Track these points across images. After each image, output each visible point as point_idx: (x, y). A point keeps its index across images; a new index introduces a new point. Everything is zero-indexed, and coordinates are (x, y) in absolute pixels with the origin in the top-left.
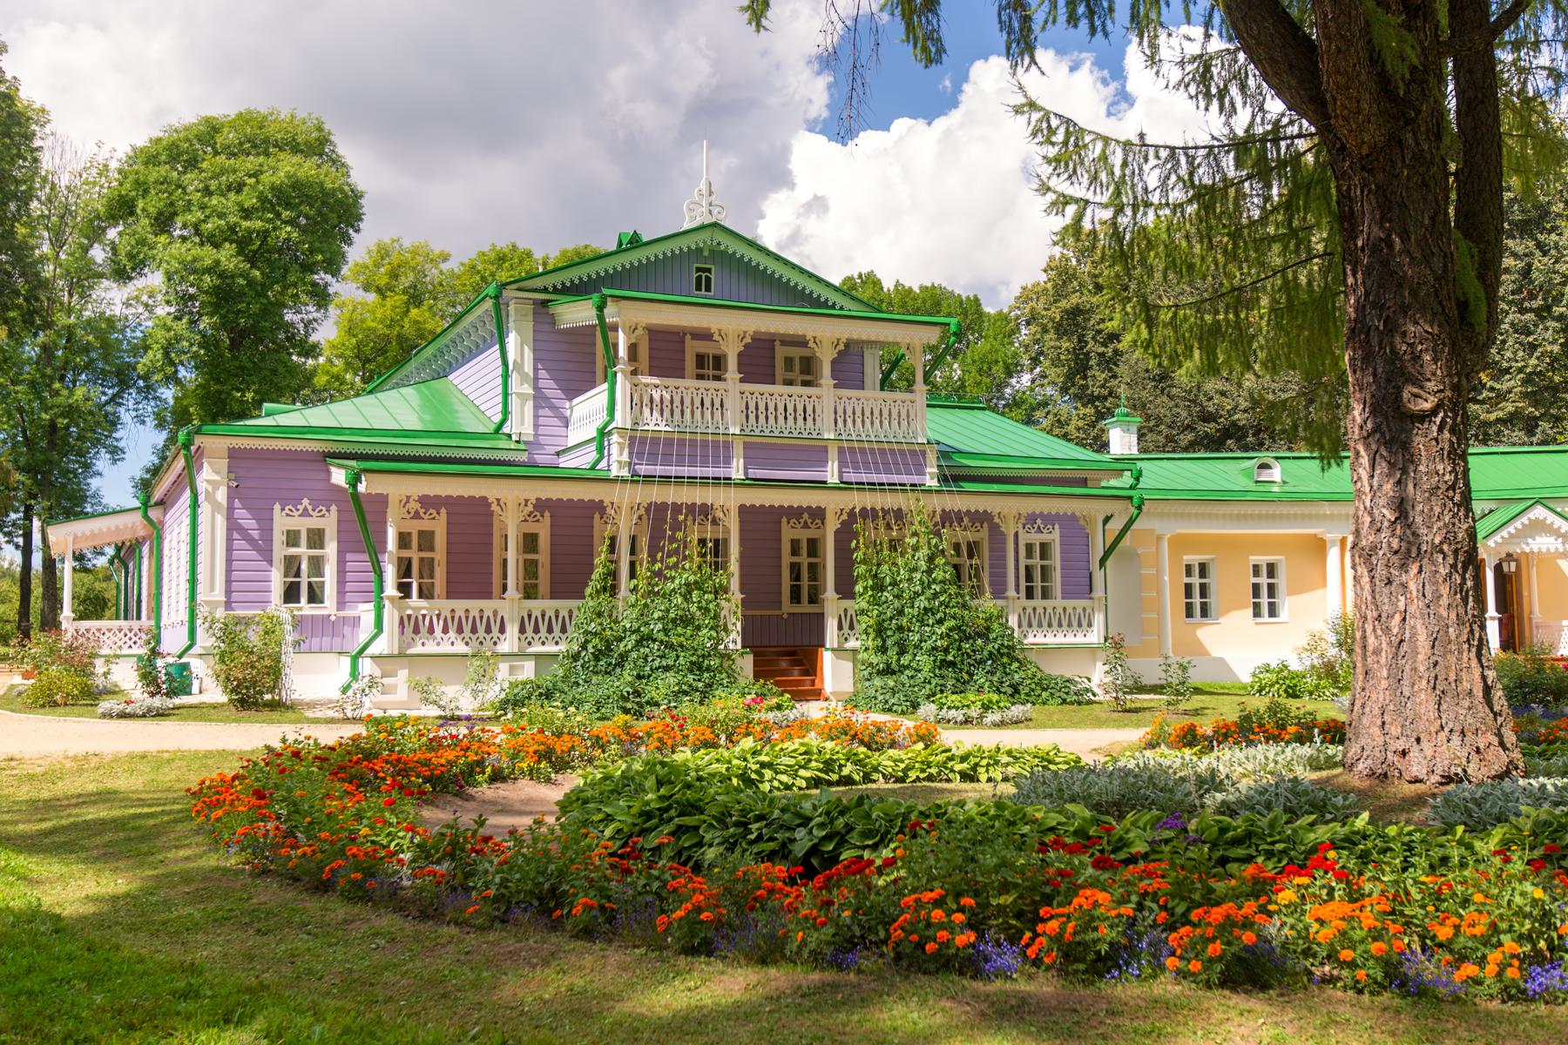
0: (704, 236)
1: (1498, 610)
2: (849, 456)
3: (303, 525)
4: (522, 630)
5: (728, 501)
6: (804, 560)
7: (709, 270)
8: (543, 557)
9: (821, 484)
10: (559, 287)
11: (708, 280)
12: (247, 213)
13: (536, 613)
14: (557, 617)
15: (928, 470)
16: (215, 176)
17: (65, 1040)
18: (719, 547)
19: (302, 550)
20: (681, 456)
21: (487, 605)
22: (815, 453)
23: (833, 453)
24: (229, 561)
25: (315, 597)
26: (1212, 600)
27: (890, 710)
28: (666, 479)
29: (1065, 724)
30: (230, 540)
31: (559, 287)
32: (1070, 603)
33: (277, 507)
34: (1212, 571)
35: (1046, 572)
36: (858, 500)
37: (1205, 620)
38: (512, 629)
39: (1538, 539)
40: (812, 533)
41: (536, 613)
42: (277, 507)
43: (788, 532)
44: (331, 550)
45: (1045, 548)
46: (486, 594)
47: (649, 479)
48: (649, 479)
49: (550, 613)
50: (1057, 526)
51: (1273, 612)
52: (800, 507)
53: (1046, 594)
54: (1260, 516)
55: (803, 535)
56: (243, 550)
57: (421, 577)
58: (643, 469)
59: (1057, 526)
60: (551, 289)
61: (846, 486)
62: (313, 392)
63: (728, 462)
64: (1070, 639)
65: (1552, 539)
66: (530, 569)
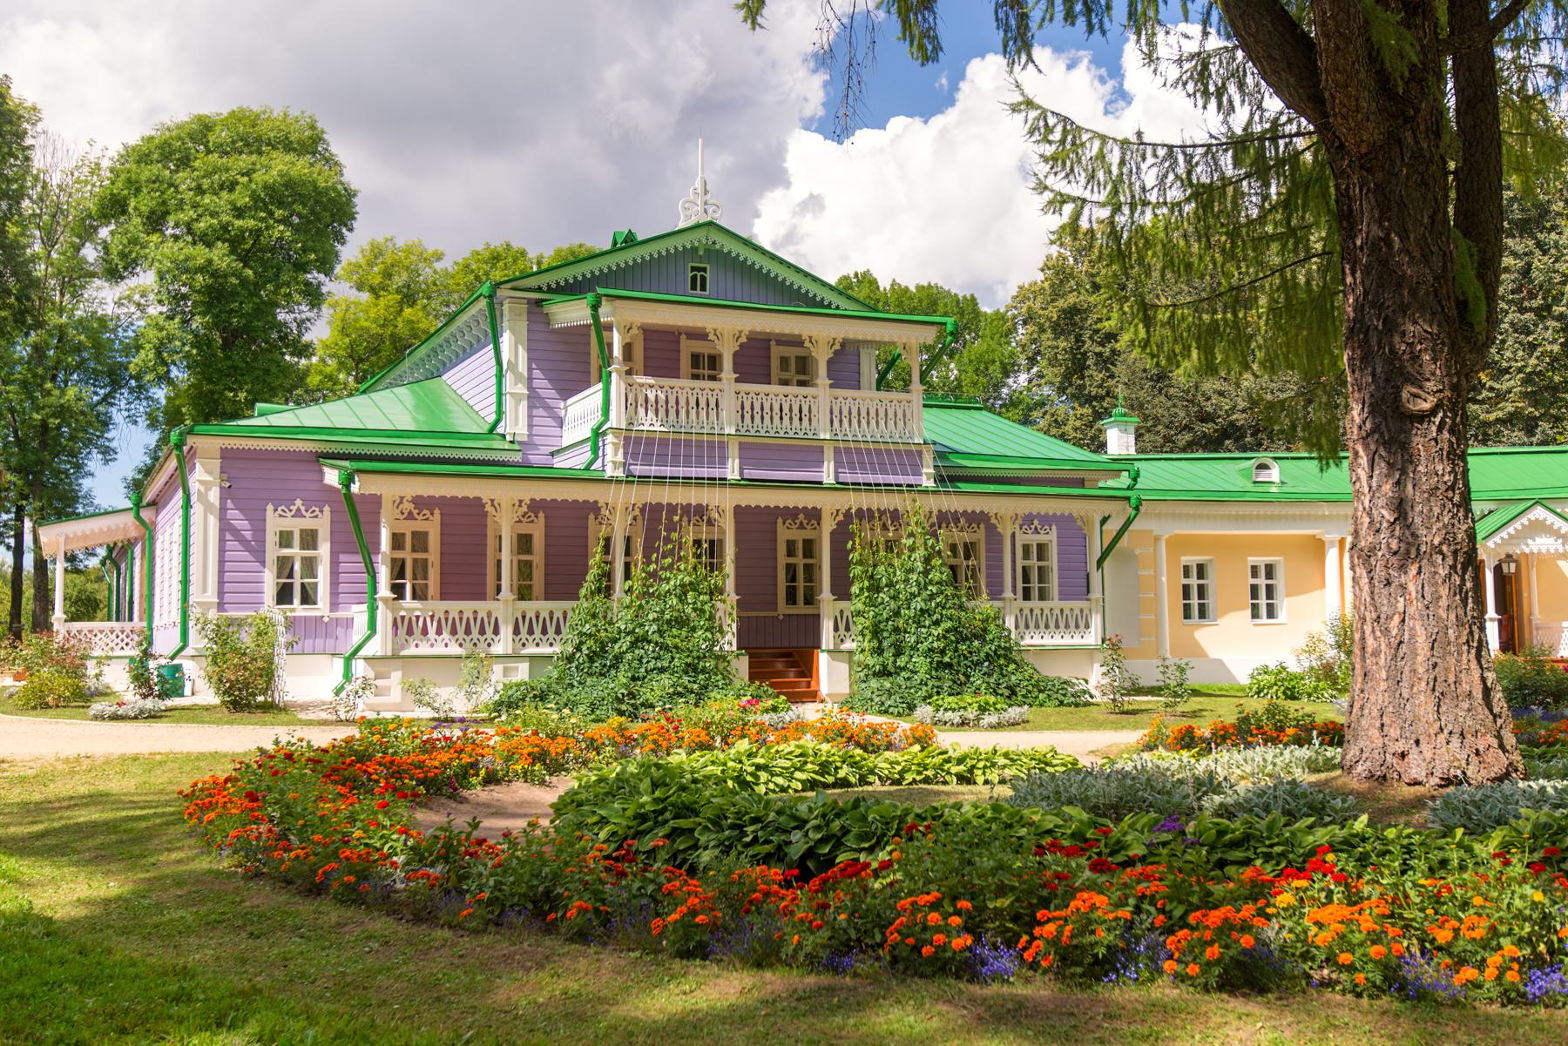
1: (1497, 612)
2: (846, 456)
3: (296, 525)
4: (516, 631)
5: (723, 502)
6: (800, 560)
7: (704, 270)
8: (538, 558)
9: (817, 485)
10: (554, 286)
11: (703, 279)
12: (239, 212)
13: (531, 614)
14: (551, 618)
15: (925, 470)
16: (208, 175)
18: (715, 548)
19: (295, 551)
20: (676, 456)
21: (482, 607)
22: (812, 454)
23: (829, 453)
24: (222, 562)
25: (308, 598)
26: (1210, 601)
27: (886, 712)
28: (660, 480)
30: (222, 550)
31: (554, 286)
32: (1067, 605)
33: (270, 508)
36: (854, 501)
37: (1203, 622)
38: (506, 631)
39: (1538, 540)
40: (807, 534)
41: (531, 614)
42: (270, 508)
43: (784, 533)
44: (324, 550)
45: (1042, 550)
47: (644, 479)
48: (644, 479)
49: (544, 614)
50: (1054, 527)
51: (1271, 613)
52: (796, 508)
53: (1043, 596)
54: (1258, 517)
55: (799, 536)
56: (236, 551)
57: (415, 578)
58: (638, 469)
59: (1054, 527)
60: (545, 288)
61: (841, 486)
62: (306, 392)
63: (723, 462)
64: (1067, 641)
65: (1552, 540)
66: (524, 570)
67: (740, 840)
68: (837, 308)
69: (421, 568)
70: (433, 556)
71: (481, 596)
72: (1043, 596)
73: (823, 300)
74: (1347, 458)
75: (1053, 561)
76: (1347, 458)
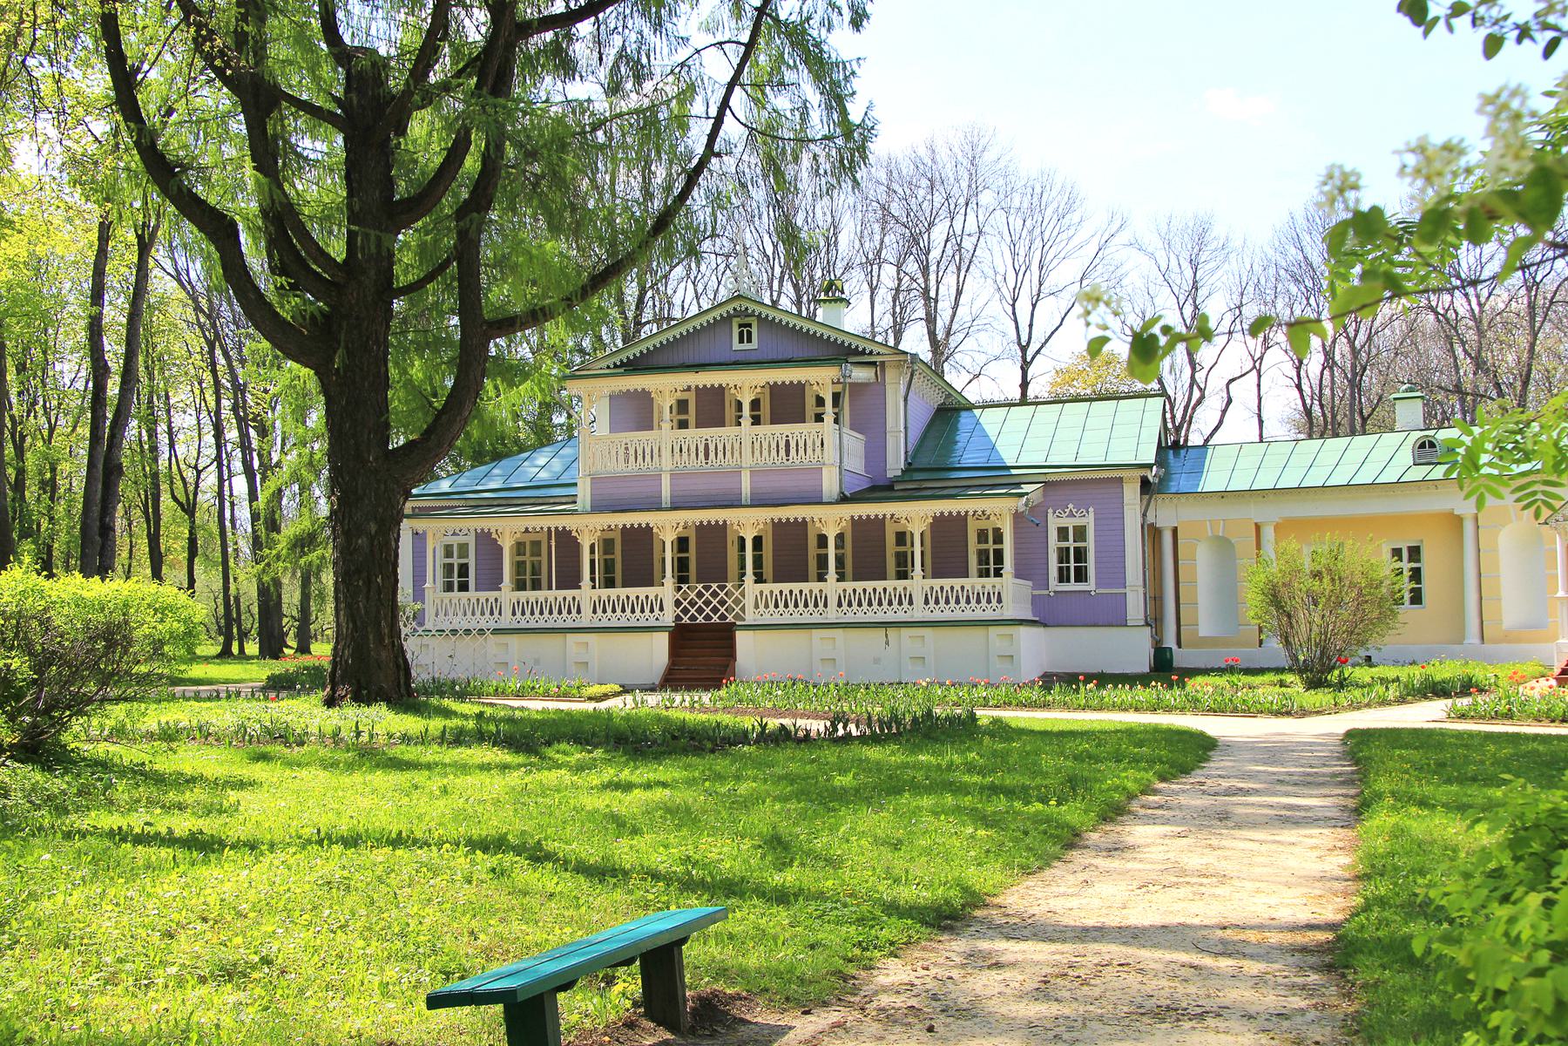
0: (736, 304)
3: (1070, 523)
6: (991, 546)
7: (750, 325)
8: (618, 556)
11: (749, 334)
13: (523, 600)
17: (1518, 1038)
18: (998, 538)
21: (651, 591)
25: (1081, 576)
27: (565, 695)
29: (1476, 742)
32: (483, 595)
34: (1425, 554)
35: (999, 556)
41: (523, 600)
45: (1080, 533)
46: (649, 582)
49: (604, 598)
50: (1091, 510)
53: (998, 574)
57: (1068, 568)
66: (758, 563)
67: (537, 796)
68: (878, 354)
69: (464, 570)
70: (471, 561)
71: (651, 584)
72: (998, 574)
73: (864, 349)
74: (379, 239)
75: (1090, 544)
76: (379, 239)
